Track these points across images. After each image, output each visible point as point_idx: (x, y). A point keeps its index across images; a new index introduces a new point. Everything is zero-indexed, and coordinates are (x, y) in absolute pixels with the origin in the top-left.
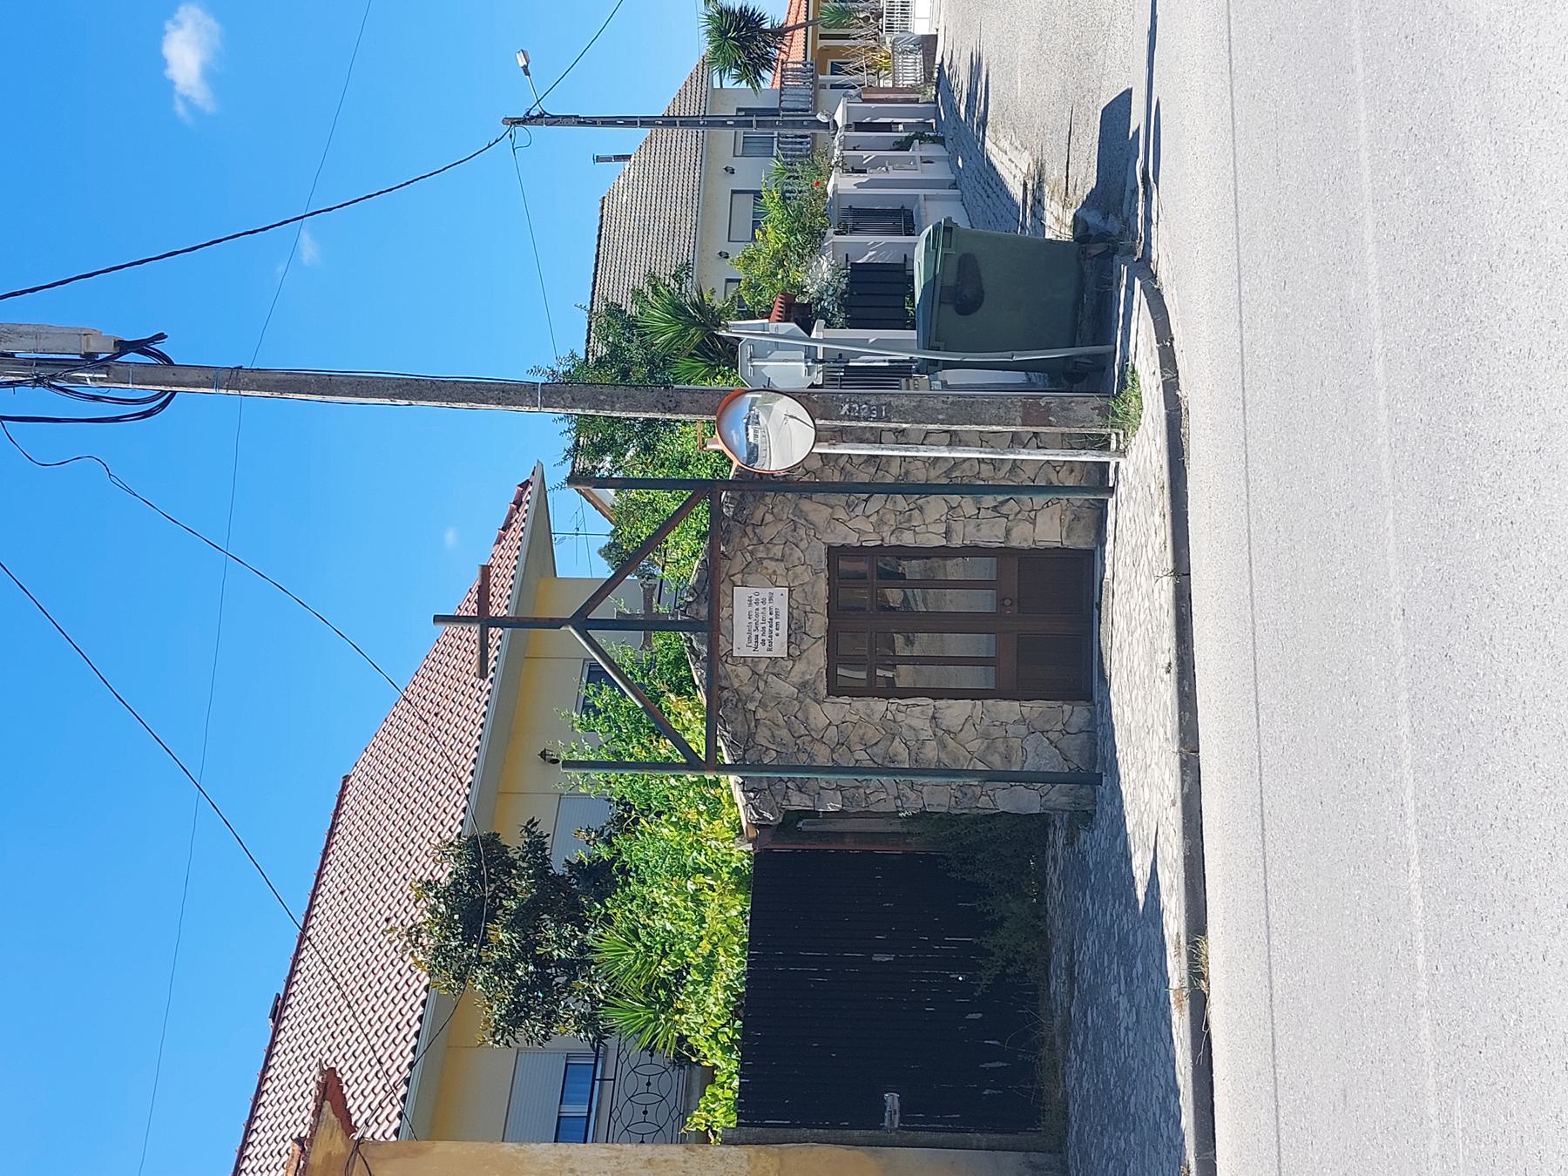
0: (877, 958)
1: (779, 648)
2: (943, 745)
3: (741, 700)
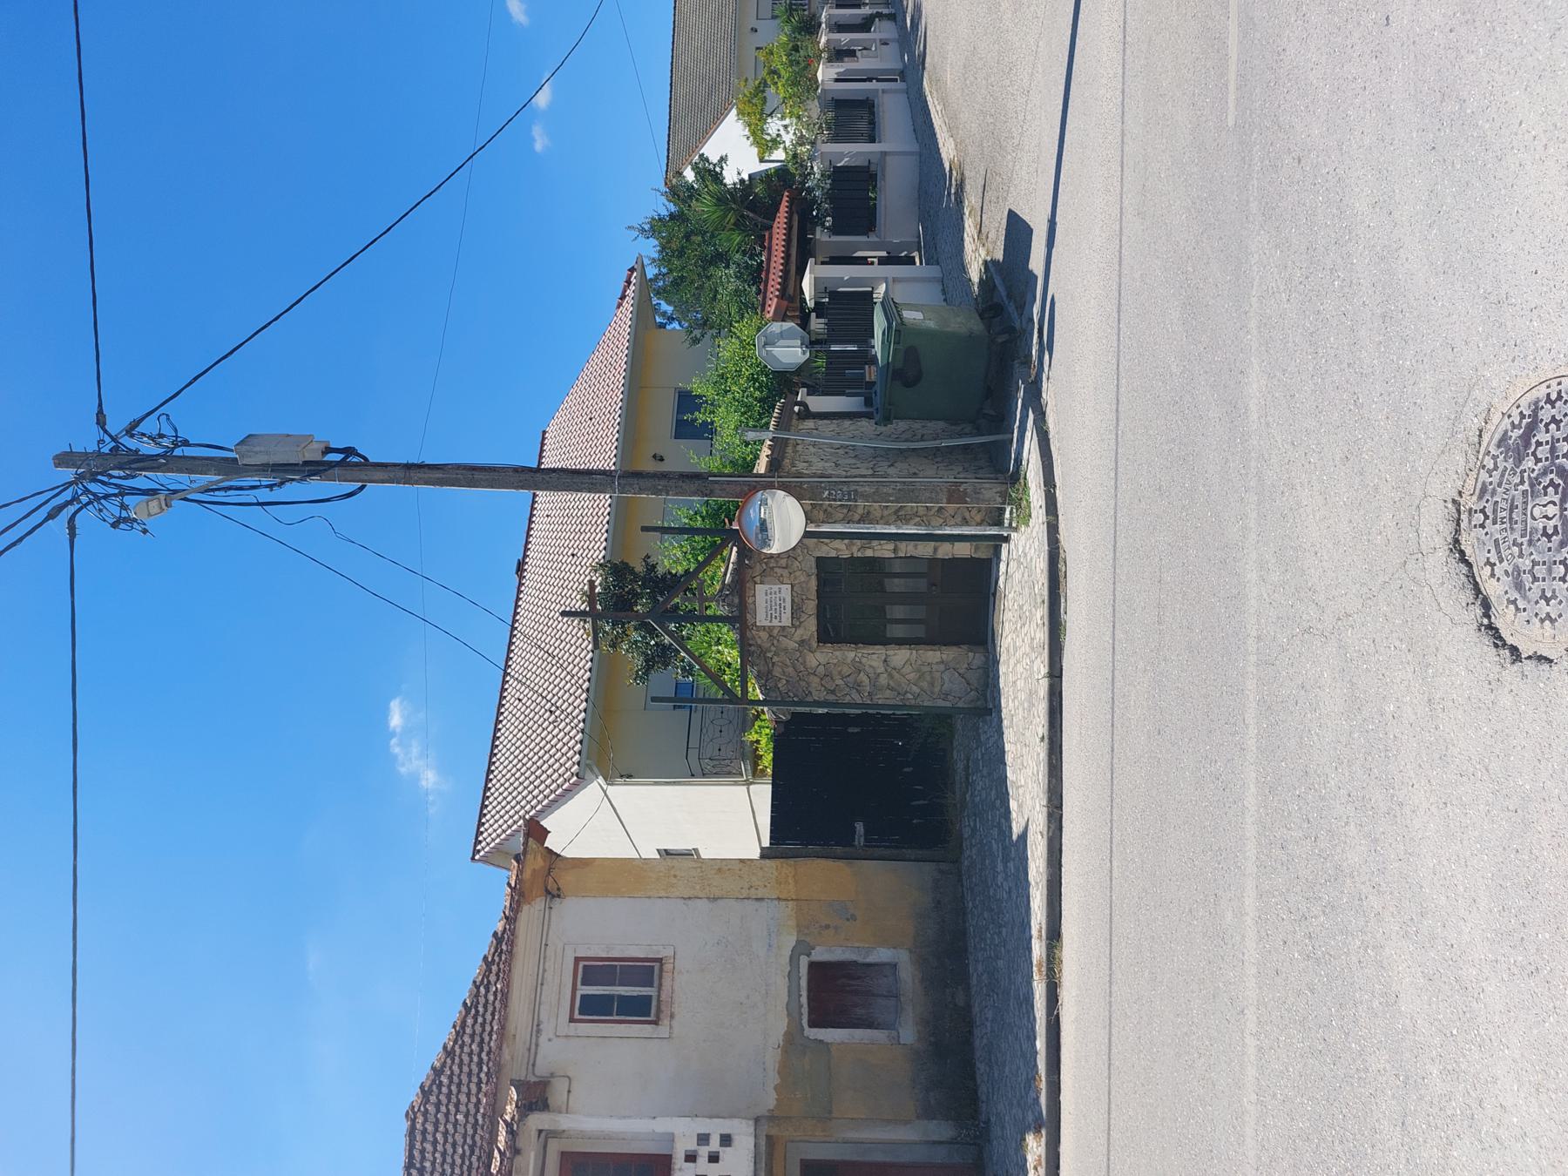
0: (851, 730)
1: (786, 620)
2: (891, 676)
3: (763, 652)
